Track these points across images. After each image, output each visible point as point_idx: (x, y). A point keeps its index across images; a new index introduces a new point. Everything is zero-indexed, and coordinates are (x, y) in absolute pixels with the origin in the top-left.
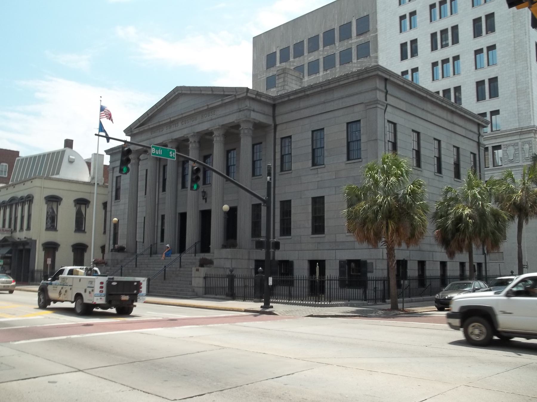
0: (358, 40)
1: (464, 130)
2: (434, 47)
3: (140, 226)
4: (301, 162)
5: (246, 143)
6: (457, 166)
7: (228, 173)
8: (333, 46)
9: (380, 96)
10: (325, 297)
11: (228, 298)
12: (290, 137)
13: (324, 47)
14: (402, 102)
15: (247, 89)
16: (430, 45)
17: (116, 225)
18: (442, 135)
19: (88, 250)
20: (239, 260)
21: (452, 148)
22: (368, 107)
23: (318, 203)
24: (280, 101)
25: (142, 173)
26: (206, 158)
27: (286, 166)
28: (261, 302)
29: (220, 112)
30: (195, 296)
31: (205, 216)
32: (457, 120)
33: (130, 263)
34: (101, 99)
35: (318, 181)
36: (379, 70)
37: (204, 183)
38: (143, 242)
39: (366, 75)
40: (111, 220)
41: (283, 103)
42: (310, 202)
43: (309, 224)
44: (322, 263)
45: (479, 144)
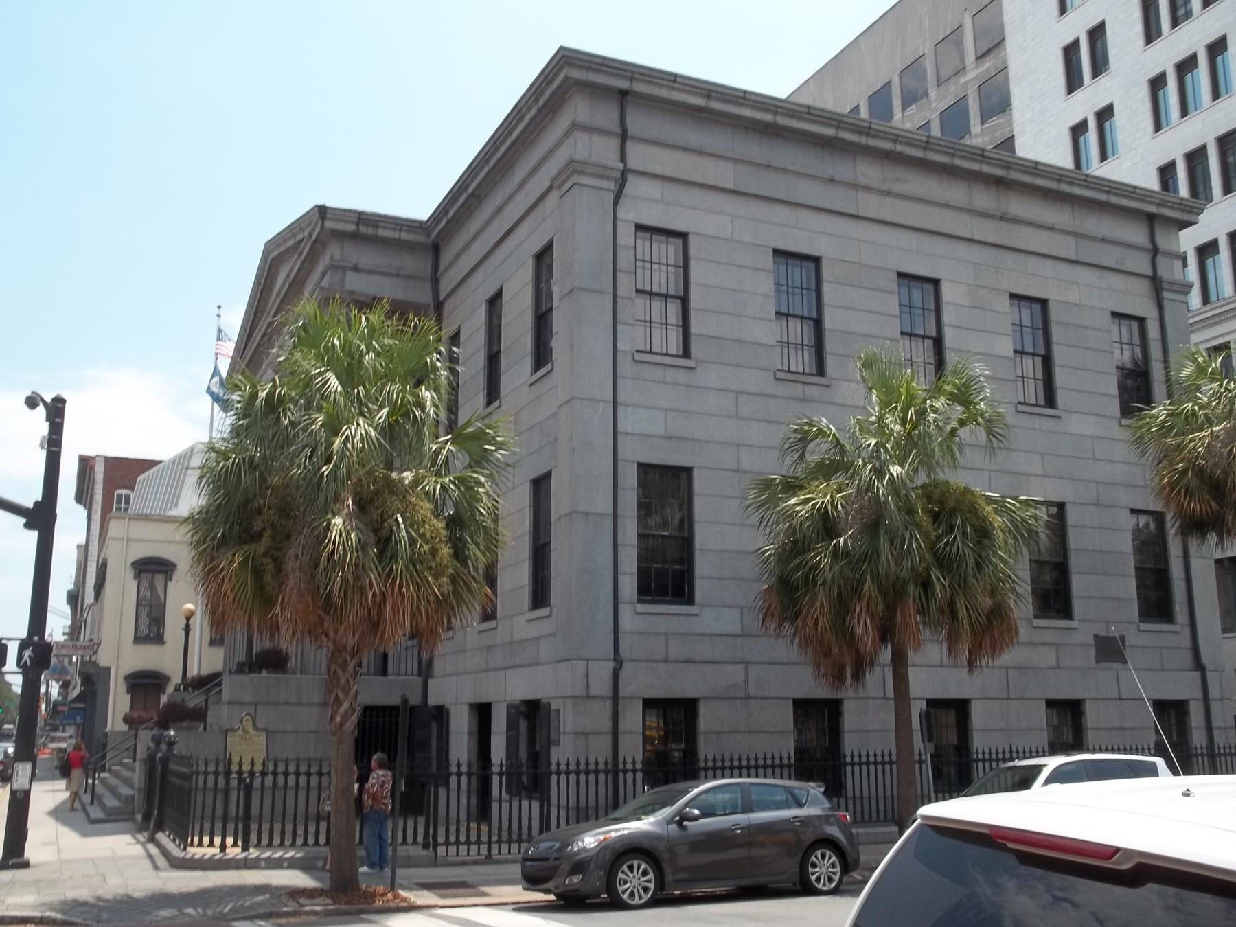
0: (981, 70)
1: (1071, 239)
8: (924, 101)
9: (604, 151)
13: (983, 122)
14: (710, 163)
32: (1018, 206)
34: (221, 312)
43: (526, 595)
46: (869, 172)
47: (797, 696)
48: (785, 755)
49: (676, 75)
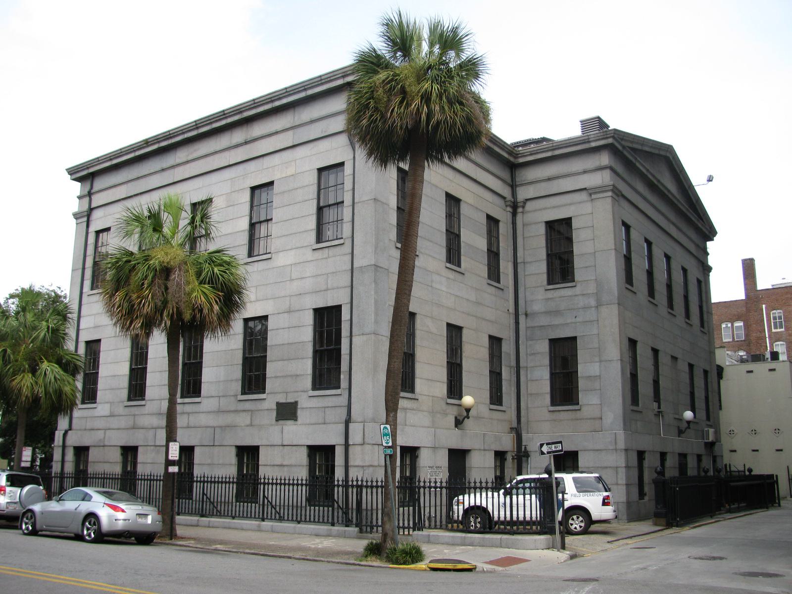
23: (328, 321)
47: (123, 444)
48: (379, 480)
49: (98, 158)
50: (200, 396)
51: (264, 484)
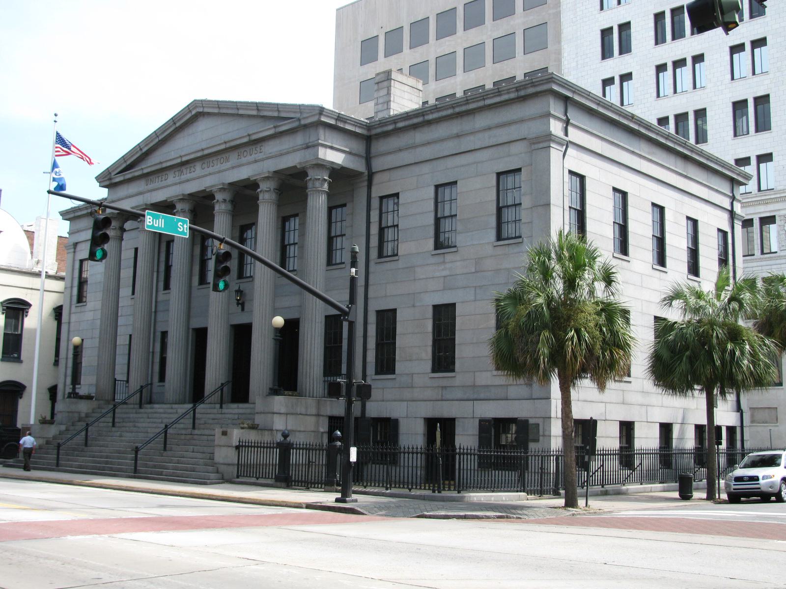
2: (659, 39)
3: (122, 351)
4: (414, 243)
5: (318, 203)
6: (694, 254)
7: (283, 264)
9: (556, 127)
10: (455, 485)
11: (278, 484)
12: (397, 195)
15: (321, 110)
16: (652, 33)
17: (78, 350)
18: (664, 197)
19: (25, 395)
20: (296, 418)
21: (684, 221)
22: (534, 147)
23: (444, 318)
24: (379, 130)
25: (127, 255)
26: (244, 229)
27: (389, 248)
28: (337, 491)
29: (271, 148)
30: (224, 480)
31: (241, 335)
33: (103, 419)
34: (57, 119)
35: (444, 277)
36: (555, 82)
37: (241, 275)
38: (127, 381)
39: (531, 90)
40: (68, 340)
41: (386, 134)
42: (430, 313)
43: (427, 353)
44: (448, 425)
45: (732, 214)
46: (419, 136)
50: (394, 373)
51: (460, 454)
